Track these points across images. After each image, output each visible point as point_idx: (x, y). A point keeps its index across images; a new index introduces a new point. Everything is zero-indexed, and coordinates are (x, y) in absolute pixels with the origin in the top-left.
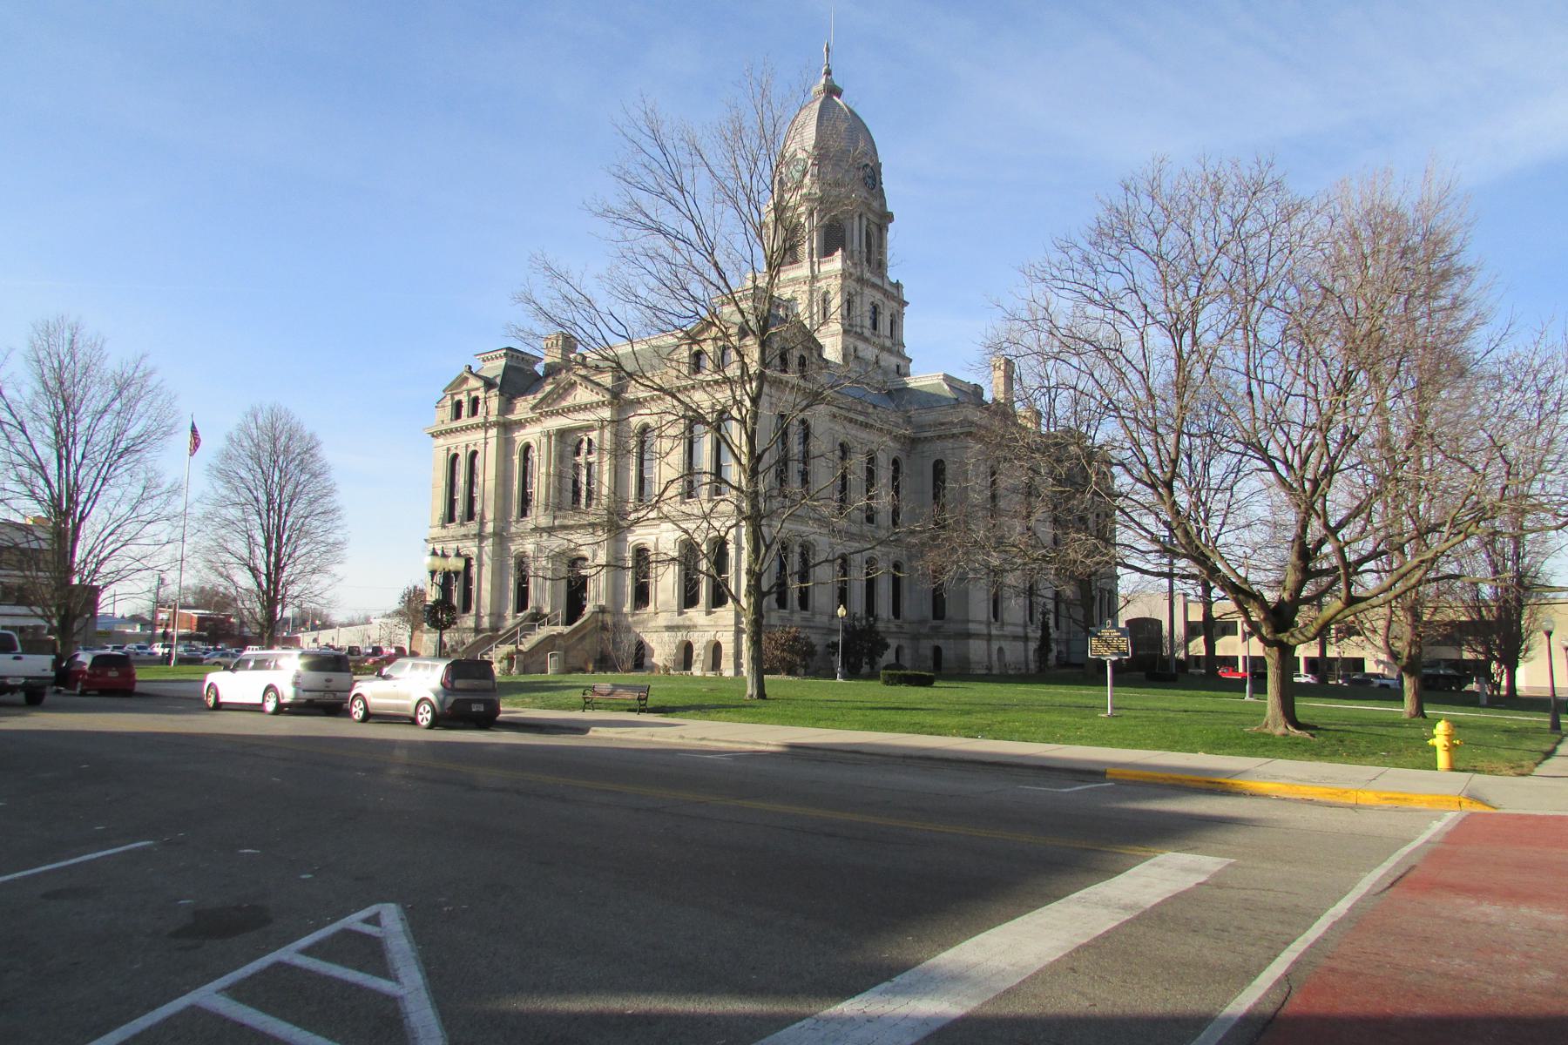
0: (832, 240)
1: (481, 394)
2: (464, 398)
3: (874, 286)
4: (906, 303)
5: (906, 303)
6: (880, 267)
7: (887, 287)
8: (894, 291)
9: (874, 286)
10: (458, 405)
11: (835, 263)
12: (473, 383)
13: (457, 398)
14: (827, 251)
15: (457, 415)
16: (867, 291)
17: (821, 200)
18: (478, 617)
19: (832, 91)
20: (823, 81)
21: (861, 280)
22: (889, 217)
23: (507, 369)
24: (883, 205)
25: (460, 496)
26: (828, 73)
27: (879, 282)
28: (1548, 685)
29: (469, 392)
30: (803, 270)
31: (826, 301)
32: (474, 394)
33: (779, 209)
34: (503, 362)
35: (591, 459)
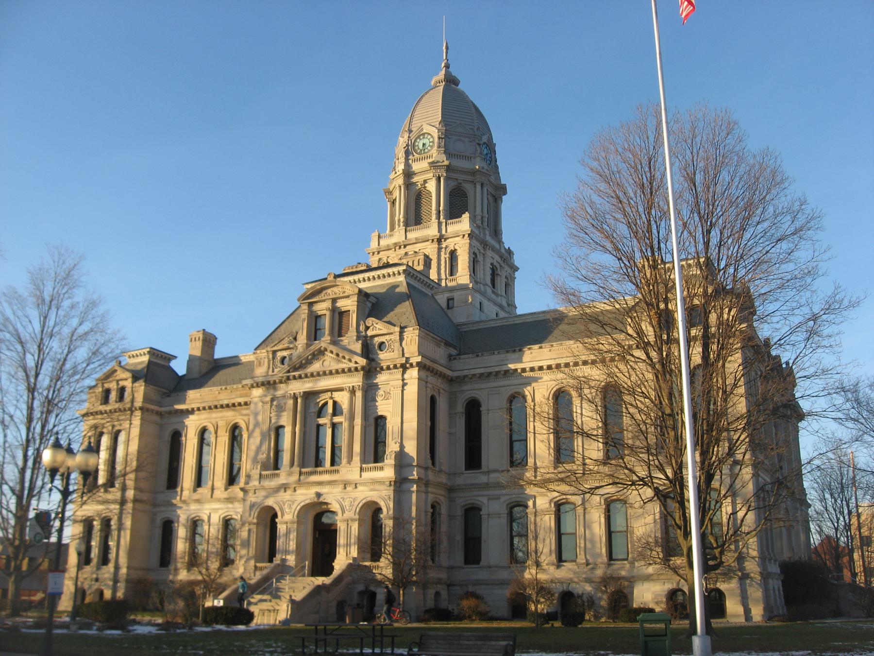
0: (455, 206)
1: (128, 384)
2: (113, 386)
3: (493, 249)
4: (517, 269)
5: (517, 269)
6: (497, 233)
7: (503, 251)
8: (506, 255)
9: (493, 249)
10: (107, 392)
11: (464, 224)
12: (121, 374)
13: (106, 386)
14: (454, 211)
15: (106, 400)
16: (489, 253)
17: (449, 168)
18: (117, 567)
19: (451, 81)
20: (443, 72)
21: (485, 244)
22: (503, 190)
23: (150, 362)
24: (498, 178)
25: (27, 485)
26: (447, 66)
27: (497, 246)
28: (491, 467)
29: (118, 381)
30: (432, 231)
31: (453, 255)
32: (122, 383)
33: (408, 174)
34: (146, 358)
35: (337, 419)
